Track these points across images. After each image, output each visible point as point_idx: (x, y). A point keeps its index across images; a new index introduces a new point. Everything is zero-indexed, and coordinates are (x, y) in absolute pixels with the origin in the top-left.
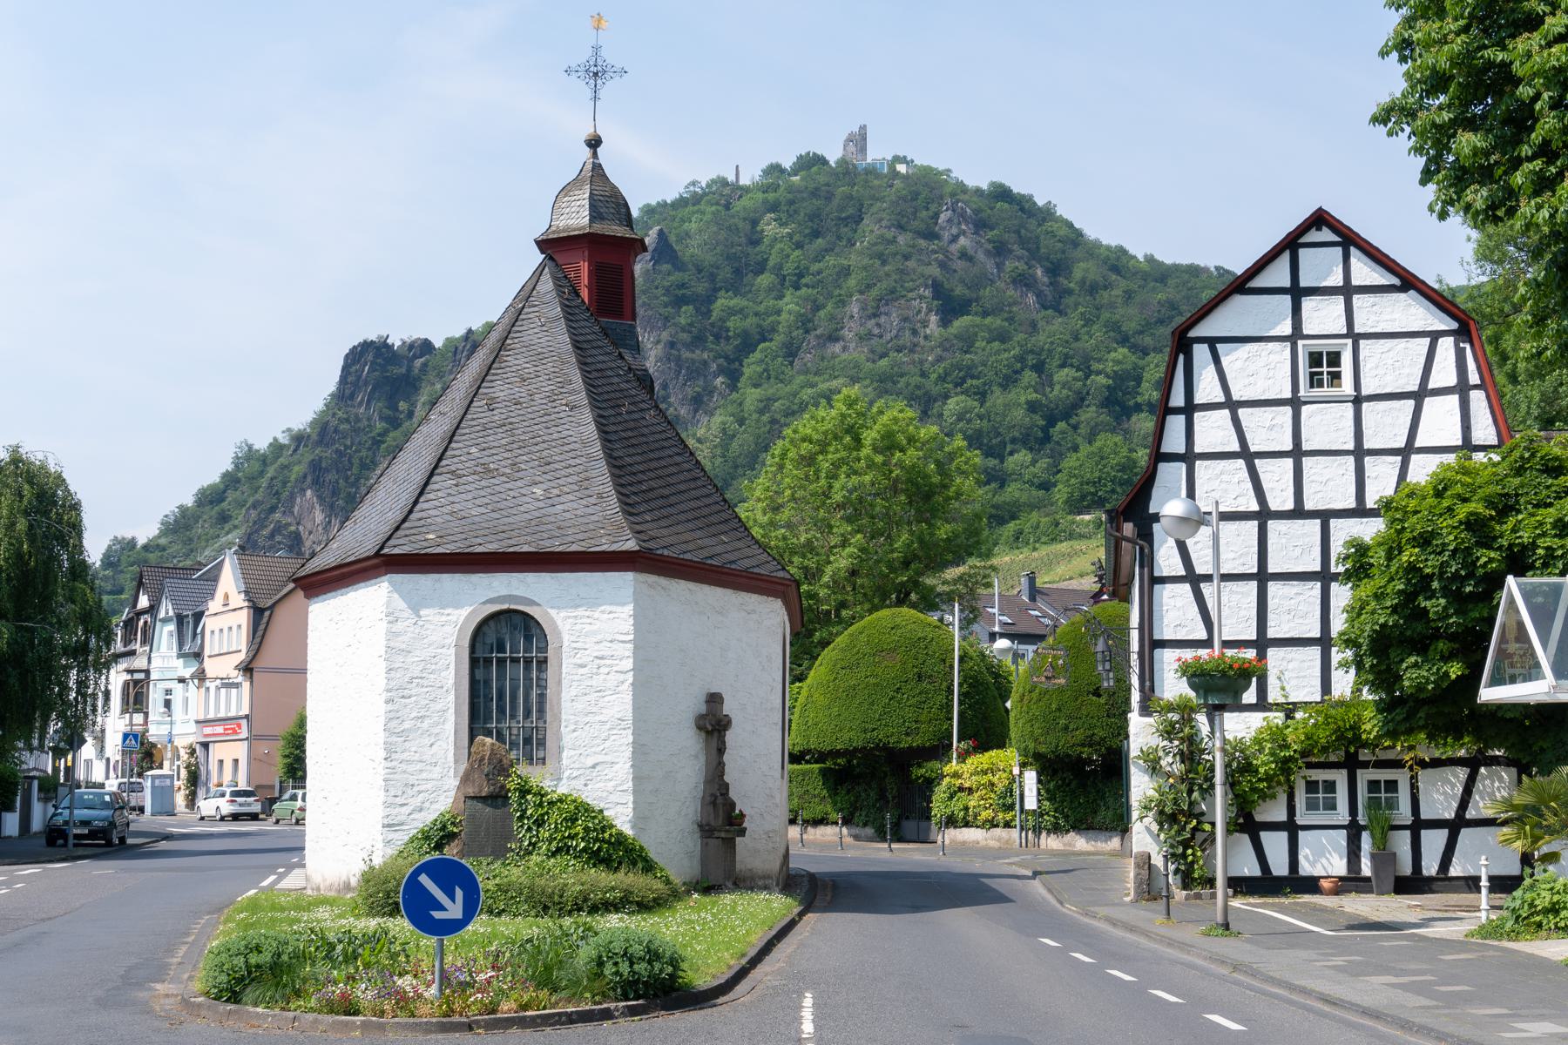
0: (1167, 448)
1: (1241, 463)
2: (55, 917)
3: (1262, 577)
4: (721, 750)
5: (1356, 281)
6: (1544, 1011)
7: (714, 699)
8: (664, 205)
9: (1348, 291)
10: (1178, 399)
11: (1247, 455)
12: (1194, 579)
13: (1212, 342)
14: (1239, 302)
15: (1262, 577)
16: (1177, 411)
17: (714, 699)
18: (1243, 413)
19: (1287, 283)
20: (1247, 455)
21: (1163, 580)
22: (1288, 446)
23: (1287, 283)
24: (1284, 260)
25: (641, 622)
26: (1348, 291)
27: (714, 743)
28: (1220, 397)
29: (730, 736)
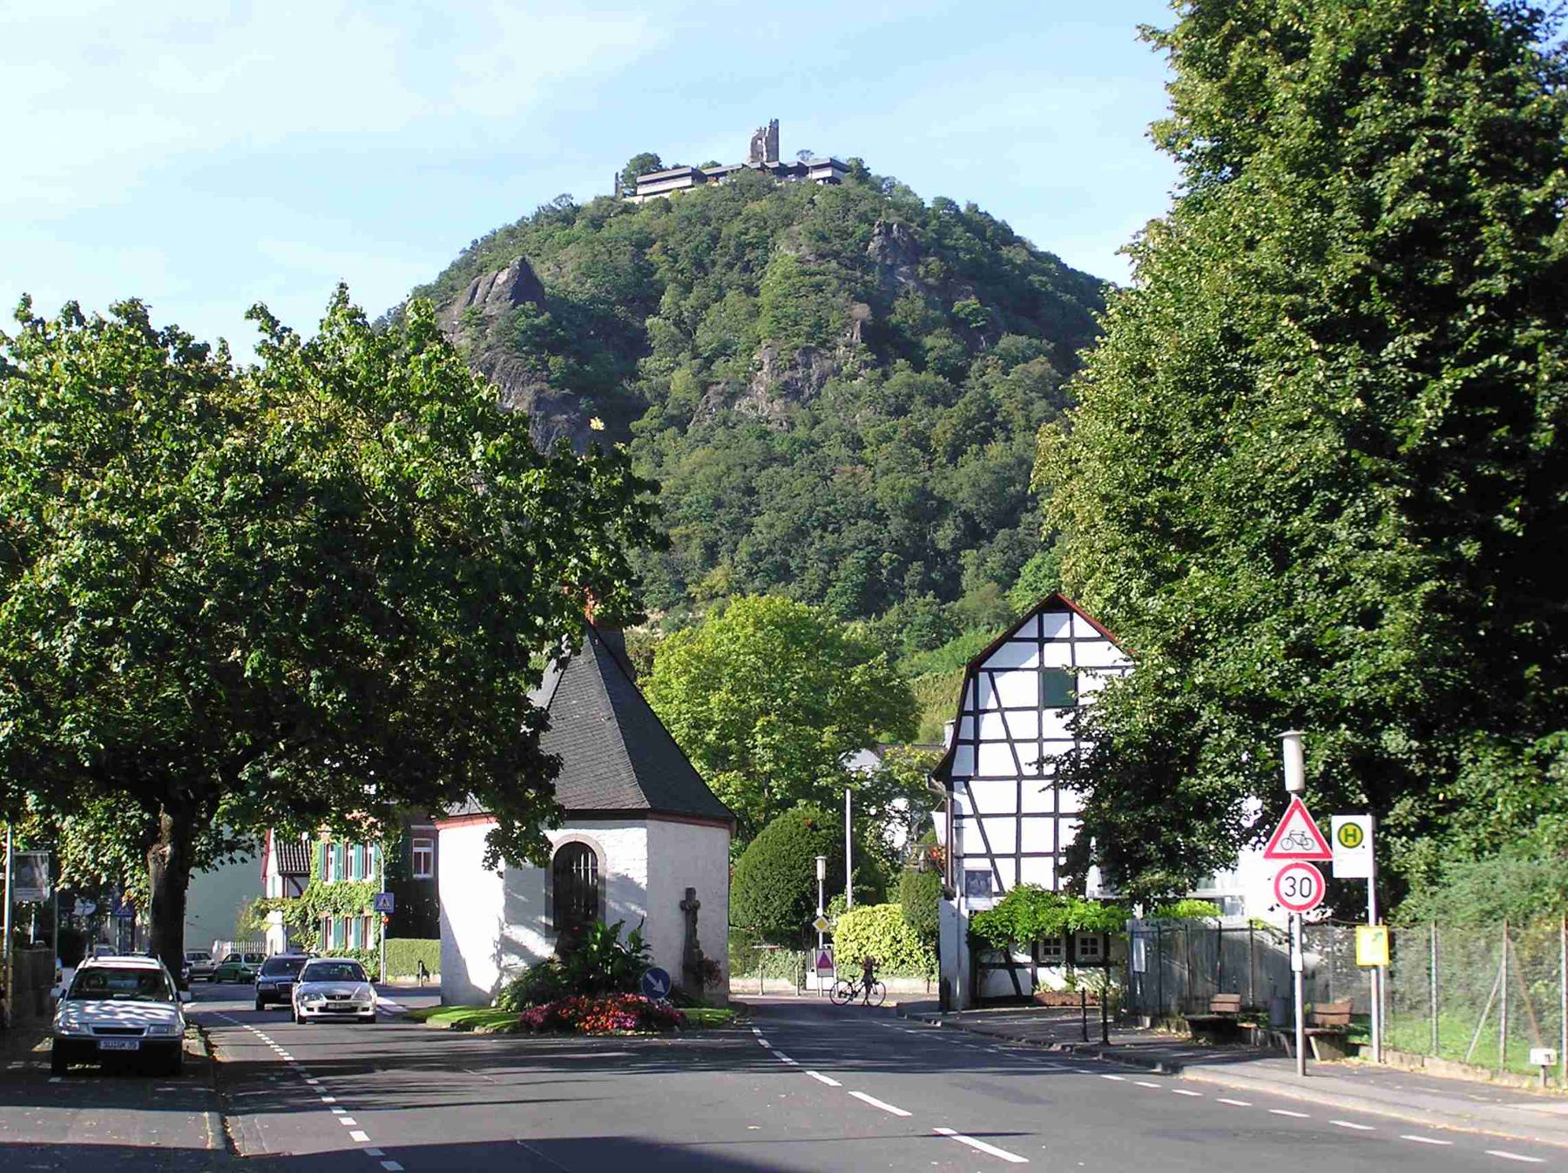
0: (966, 709)
1: (981, 811)
2: (1038, 1101)
3: (1019, 815)
4: (695, 921)
5: (1077, 634)
6: (725, 1062)
7: (690, 892)
8: (522, 223)
9: (1072, 640)
10: (969, 706)
11: (1010, 741)
12: (979, 817)
13: (991, 671)
14: (1008, 646)
15: (1019, 815)
16: (968, 713)
17: (690, 892)
18: (1007, 714)
19: (1036, 635)
20: (1010, 741)
21: (986, 711)
22: (1035, 736)
23: (1036, 635)
24: (1035, 620)
25: (650, 845)
26: (1072, 640)
27: (691, 916)
28: (996, 706)
29: (699, 913)
